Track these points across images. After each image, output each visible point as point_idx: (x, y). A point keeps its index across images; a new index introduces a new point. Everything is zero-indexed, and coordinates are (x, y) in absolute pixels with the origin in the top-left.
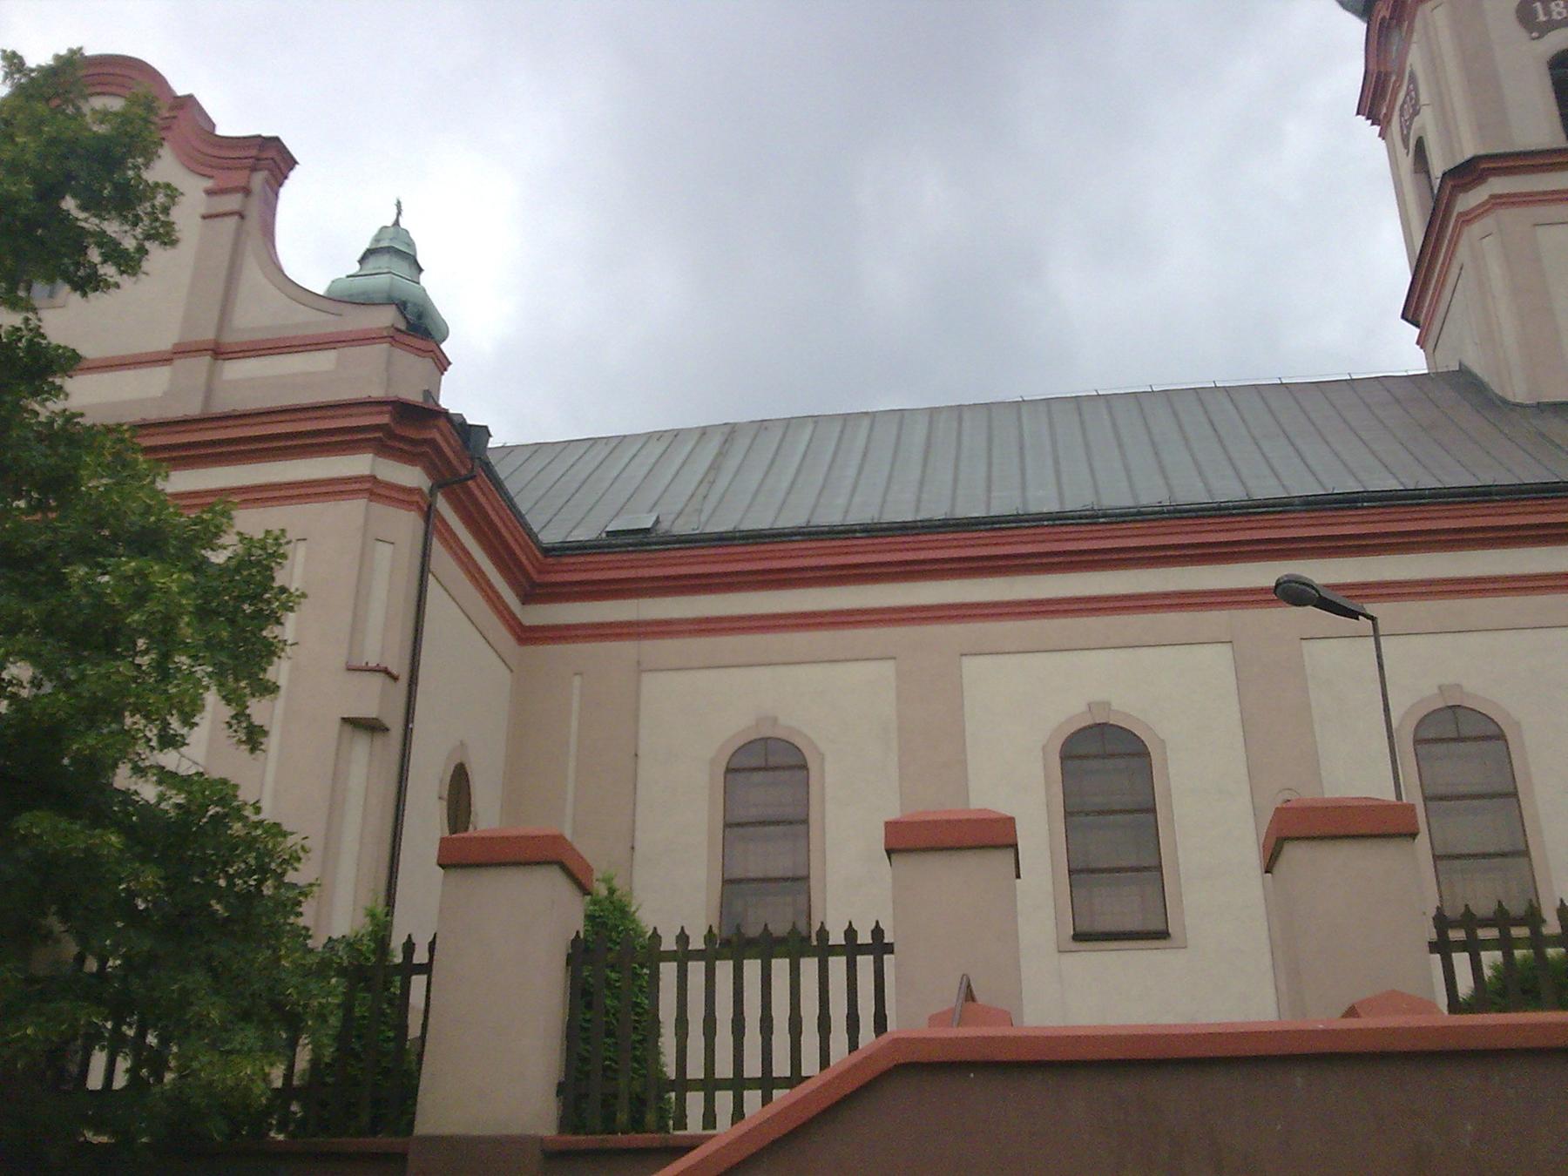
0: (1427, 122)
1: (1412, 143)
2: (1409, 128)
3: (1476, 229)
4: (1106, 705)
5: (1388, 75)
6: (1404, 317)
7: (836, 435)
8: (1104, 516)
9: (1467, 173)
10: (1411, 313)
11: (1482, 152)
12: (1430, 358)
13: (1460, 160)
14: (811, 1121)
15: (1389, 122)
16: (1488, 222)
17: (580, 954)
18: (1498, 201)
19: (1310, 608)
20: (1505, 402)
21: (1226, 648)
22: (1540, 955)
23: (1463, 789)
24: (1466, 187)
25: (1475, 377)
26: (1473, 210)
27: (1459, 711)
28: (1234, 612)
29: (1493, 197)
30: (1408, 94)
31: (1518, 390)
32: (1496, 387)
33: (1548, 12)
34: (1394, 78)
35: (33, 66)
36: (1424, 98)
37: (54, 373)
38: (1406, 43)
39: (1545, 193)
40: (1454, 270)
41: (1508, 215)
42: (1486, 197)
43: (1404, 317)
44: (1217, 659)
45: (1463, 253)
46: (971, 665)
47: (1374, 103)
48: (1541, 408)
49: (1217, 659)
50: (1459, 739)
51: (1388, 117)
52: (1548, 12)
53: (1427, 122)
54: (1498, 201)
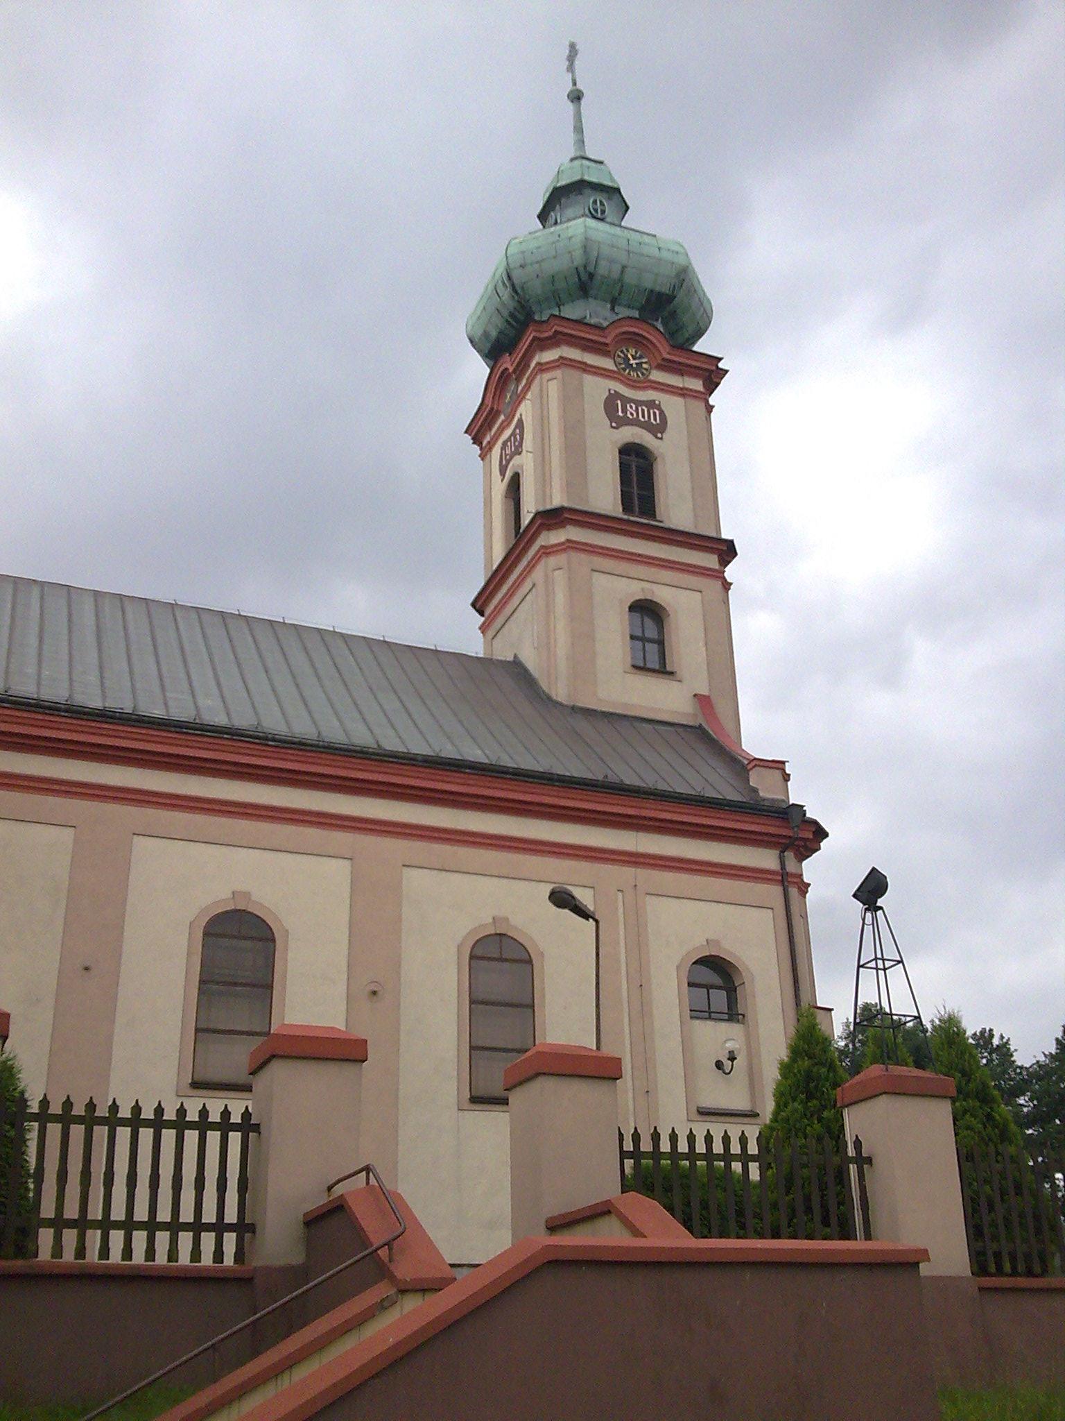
0: (526, 462)
1: (509, 474)
2: (508, 462)
3: (552, 561)
4: (247, 895)
5: (498, 413)
6: (473, 605)
7: (9, 598)
8: (274, 740)
9: (552, 518)
10: (479, 605)
11: (566, 505)
12: (489, 644)
13: (549, 507)
14: (845, 1265)
15: (491, 449)
16: (561, 559)
17: (156, 1110)
18: (571, 545)
19: (566, 911)
20: (549, 698)
21: (347, 863)
22: (693, 1165)
23: (493, 998)
24: (549, 528)
25: (526, 670)
26: (553, 546)
27: (504, 939)
28: (357, 836)
29: (568, 541)
30: (513, 434)
31: (560, 693)
32: (544, 684)
33: (624, 410)
34: (502, 417)
35: (1019, 1063)
36: (528, 444)
37: (827, 1041)
38: (519, 399)
39: (602, 548)
40: (527, 585)
41: (577, 557)
42: (563, 539)
43: (473, 605)
44: (338, 871)
45: (538, 574)
46: (142, 845)
47: (481, 428)
48: (575, 709)
49: (338, 871)
50: (501, 960)
51: (491, 445)
52: (624, 410)
53: (526, 462)
54: (571, 545)
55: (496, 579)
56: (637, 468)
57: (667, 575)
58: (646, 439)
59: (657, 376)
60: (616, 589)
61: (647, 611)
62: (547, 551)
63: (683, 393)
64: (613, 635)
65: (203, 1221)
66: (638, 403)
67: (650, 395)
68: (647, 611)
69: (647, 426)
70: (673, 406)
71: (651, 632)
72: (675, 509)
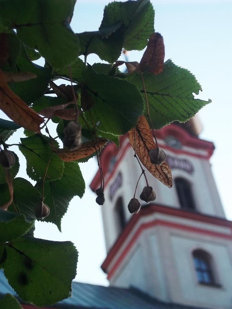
1: (115, 198)
3: (148, 231)
38: (116, 164)
45: (141, 239)
54: (156, 223)
55: (112, 253)
56: (184, 189)
57: (207, 238)
58: (185, 175)
59: (186, 149)
60: (182, 245)
61: (201, 256)
62: (145, 226)
63: (199, 156)
64: (186, 269)
65: (63, 148)
66: (180, 160)
67: (182, 157)
68: (201, 256)
69: (185, 170)
70: (195, 162)
71: (204, 267)
72: (204, 206)
